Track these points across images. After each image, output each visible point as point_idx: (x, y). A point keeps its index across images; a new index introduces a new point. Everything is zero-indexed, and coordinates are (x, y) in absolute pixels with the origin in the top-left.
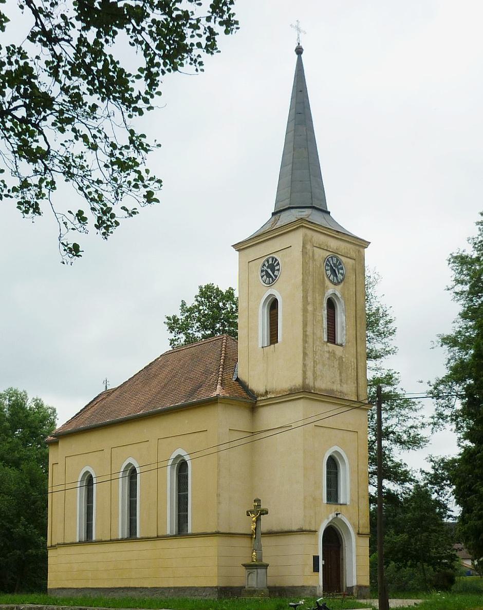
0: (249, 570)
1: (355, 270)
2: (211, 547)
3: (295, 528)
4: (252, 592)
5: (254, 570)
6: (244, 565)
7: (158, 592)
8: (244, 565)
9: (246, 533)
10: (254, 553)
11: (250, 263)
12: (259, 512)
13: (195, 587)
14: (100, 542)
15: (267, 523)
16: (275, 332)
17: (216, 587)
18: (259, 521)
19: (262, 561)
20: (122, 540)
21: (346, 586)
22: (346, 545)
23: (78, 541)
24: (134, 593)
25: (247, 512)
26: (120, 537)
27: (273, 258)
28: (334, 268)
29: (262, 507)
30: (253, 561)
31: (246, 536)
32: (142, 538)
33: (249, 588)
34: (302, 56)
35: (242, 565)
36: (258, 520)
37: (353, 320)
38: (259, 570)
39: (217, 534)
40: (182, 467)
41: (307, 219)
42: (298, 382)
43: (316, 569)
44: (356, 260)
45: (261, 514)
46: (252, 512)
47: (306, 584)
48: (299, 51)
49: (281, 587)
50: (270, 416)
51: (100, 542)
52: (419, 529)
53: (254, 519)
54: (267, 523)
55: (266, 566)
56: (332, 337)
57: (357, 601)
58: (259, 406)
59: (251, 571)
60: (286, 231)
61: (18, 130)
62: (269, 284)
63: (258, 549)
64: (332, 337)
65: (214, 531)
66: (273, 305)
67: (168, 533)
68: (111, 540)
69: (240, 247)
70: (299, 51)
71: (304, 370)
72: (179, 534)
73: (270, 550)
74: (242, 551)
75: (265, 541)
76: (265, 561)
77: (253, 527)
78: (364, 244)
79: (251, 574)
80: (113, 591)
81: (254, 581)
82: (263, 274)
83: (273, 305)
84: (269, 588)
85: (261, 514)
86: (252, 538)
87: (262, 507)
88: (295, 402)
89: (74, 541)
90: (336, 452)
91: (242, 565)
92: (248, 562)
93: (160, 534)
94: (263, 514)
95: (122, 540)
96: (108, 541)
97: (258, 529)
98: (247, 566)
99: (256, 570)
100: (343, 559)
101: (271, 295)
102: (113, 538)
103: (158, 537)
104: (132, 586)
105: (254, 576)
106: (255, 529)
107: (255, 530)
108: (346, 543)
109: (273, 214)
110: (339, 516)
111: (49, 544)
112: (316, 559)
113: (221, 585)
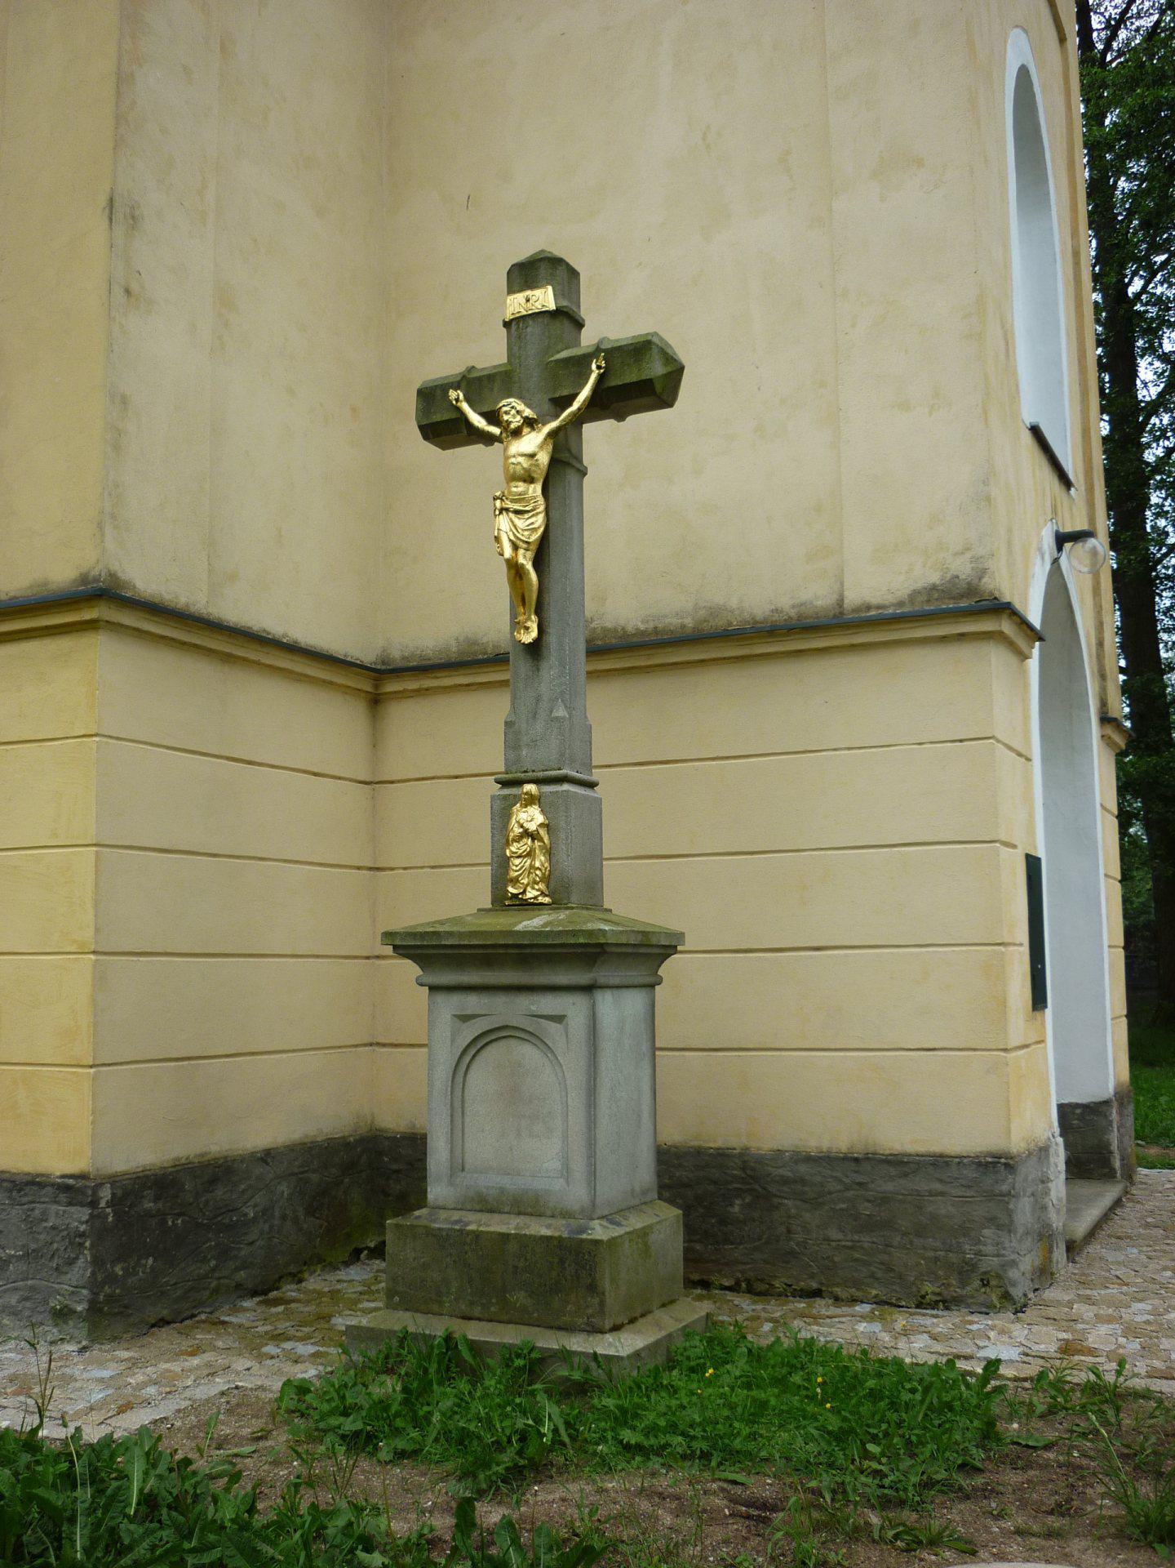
0: (472, 1003)
3: (876, 582)
17: (73, 1189)
18: (572, 476)
19: (593, 900)
29: (606, 322)
30: (523, 905)
31: (339, 678)
33: (486, 1205)
41: (1097, 619)
49: (722, 1156)
52: (1135, 167)
55: (647, 954)
61: (1111, 62)
63: (546, 773)
73: (685, 810)
75: (620, 722)
76: (629, 900)
79: (492, 1053)
92: (458, 901)
106: (542, 553)
107: (539, 562)
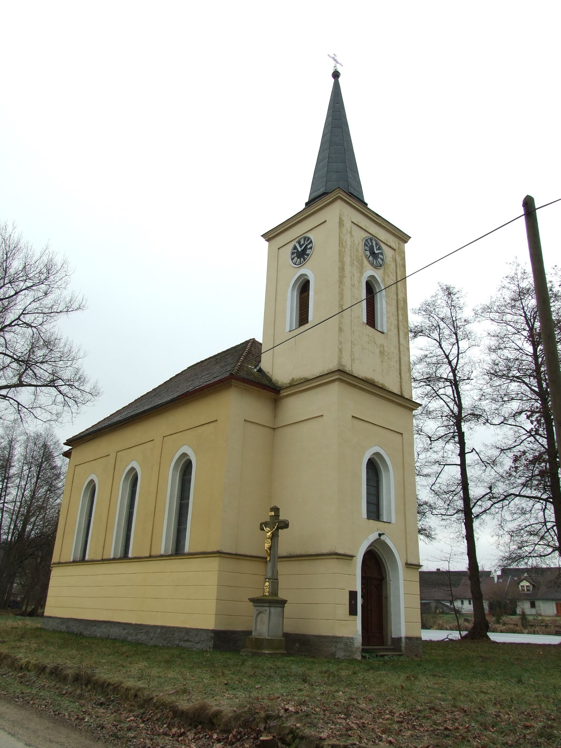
0: (258, 608)
1: (396, 260)
2: (208, 573)
4: (259, 643)
5: (265, 608)
6: (252, 600)
7: (142, 631)
8: (252, 600)
9: (254, 554)
10: (267, 584)
11: (280, 249)
12: (277, 524)
13: (186, 628)
14: (138, 559)
15: (288, 542)
16: (305, 316)
17: (212, 631)
20: (120, 559)
21: (391, 637)
22: (391, 579)
23: (72, 560)
24: (117, 630)
25: (261, 524)
26: (112, 557)
27: (305, 238)
28: (373, 251)
29: (281, 518)
32: (135, 558)
34: (340, 79)
35: (249, 599)
36: (274, 536)
37: (394, 309)
38: (273, 609)
39: (219, 554)
40: (186, 468)
42: (333, 365)
43: (353, 611)
44: (397, 250)
45: (278, 528)
46: (266, 524)
47: (338, 634)
48: (336, 75)
49: (304, 635)
50: (296, 407)
51: (138, 559)
53: (269, 534)
54: (288, 542)
55: (283, 603)
56: (371, 321)
57: (403, 649)
58: (284, 396)
59: (262, 609)
60: (322, 205)
62: (300, 264)
64: (371, 321)
65: (215, 550)
66: (304, 288)
67: (162, 552)
68: (103, 560)
69: (269, 236)
70: (336, 75)
71: (340, 347)
72: (125, 557)
74: (253, 582)
76: (282, 595)
77: (267, 545)
78: (404, 238)
80: (96, 625)
81: (263, 626)
82: (293, 256)
83: (304, 288)
84: (286, 635)
85: (278, 528)
86: (266, 562)
87: (281, 518)
88: (303, 552)
89: (68, 561)
90: (377, 454)
91: (249, 599)
92: (257, 594)
93: (153, 554)
94: (282, 528)
95: (120, 559)
96: (99, 561)
97: (271, 549)
98: (256, 601)
99: (268, 609)
100: (386, 598)
101: (302, 276)
102: (105, 557)
103: (150, 557)
104: (116, 620)
105: (265, 617)
106: (270, 548)
108: (391, 575)
109: (307, 204)
110: (382, 537)
111: (55, 559)
112: (353, 595)
113: (222, 627)
